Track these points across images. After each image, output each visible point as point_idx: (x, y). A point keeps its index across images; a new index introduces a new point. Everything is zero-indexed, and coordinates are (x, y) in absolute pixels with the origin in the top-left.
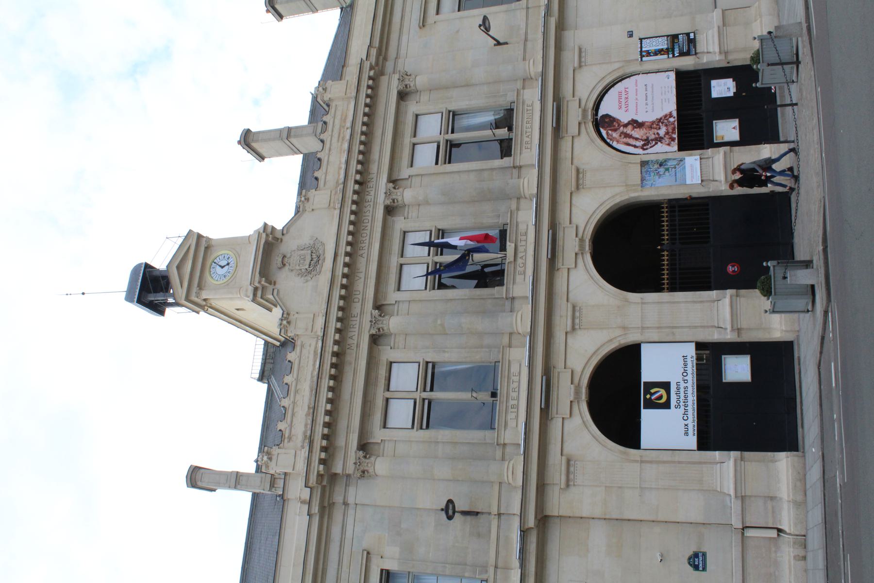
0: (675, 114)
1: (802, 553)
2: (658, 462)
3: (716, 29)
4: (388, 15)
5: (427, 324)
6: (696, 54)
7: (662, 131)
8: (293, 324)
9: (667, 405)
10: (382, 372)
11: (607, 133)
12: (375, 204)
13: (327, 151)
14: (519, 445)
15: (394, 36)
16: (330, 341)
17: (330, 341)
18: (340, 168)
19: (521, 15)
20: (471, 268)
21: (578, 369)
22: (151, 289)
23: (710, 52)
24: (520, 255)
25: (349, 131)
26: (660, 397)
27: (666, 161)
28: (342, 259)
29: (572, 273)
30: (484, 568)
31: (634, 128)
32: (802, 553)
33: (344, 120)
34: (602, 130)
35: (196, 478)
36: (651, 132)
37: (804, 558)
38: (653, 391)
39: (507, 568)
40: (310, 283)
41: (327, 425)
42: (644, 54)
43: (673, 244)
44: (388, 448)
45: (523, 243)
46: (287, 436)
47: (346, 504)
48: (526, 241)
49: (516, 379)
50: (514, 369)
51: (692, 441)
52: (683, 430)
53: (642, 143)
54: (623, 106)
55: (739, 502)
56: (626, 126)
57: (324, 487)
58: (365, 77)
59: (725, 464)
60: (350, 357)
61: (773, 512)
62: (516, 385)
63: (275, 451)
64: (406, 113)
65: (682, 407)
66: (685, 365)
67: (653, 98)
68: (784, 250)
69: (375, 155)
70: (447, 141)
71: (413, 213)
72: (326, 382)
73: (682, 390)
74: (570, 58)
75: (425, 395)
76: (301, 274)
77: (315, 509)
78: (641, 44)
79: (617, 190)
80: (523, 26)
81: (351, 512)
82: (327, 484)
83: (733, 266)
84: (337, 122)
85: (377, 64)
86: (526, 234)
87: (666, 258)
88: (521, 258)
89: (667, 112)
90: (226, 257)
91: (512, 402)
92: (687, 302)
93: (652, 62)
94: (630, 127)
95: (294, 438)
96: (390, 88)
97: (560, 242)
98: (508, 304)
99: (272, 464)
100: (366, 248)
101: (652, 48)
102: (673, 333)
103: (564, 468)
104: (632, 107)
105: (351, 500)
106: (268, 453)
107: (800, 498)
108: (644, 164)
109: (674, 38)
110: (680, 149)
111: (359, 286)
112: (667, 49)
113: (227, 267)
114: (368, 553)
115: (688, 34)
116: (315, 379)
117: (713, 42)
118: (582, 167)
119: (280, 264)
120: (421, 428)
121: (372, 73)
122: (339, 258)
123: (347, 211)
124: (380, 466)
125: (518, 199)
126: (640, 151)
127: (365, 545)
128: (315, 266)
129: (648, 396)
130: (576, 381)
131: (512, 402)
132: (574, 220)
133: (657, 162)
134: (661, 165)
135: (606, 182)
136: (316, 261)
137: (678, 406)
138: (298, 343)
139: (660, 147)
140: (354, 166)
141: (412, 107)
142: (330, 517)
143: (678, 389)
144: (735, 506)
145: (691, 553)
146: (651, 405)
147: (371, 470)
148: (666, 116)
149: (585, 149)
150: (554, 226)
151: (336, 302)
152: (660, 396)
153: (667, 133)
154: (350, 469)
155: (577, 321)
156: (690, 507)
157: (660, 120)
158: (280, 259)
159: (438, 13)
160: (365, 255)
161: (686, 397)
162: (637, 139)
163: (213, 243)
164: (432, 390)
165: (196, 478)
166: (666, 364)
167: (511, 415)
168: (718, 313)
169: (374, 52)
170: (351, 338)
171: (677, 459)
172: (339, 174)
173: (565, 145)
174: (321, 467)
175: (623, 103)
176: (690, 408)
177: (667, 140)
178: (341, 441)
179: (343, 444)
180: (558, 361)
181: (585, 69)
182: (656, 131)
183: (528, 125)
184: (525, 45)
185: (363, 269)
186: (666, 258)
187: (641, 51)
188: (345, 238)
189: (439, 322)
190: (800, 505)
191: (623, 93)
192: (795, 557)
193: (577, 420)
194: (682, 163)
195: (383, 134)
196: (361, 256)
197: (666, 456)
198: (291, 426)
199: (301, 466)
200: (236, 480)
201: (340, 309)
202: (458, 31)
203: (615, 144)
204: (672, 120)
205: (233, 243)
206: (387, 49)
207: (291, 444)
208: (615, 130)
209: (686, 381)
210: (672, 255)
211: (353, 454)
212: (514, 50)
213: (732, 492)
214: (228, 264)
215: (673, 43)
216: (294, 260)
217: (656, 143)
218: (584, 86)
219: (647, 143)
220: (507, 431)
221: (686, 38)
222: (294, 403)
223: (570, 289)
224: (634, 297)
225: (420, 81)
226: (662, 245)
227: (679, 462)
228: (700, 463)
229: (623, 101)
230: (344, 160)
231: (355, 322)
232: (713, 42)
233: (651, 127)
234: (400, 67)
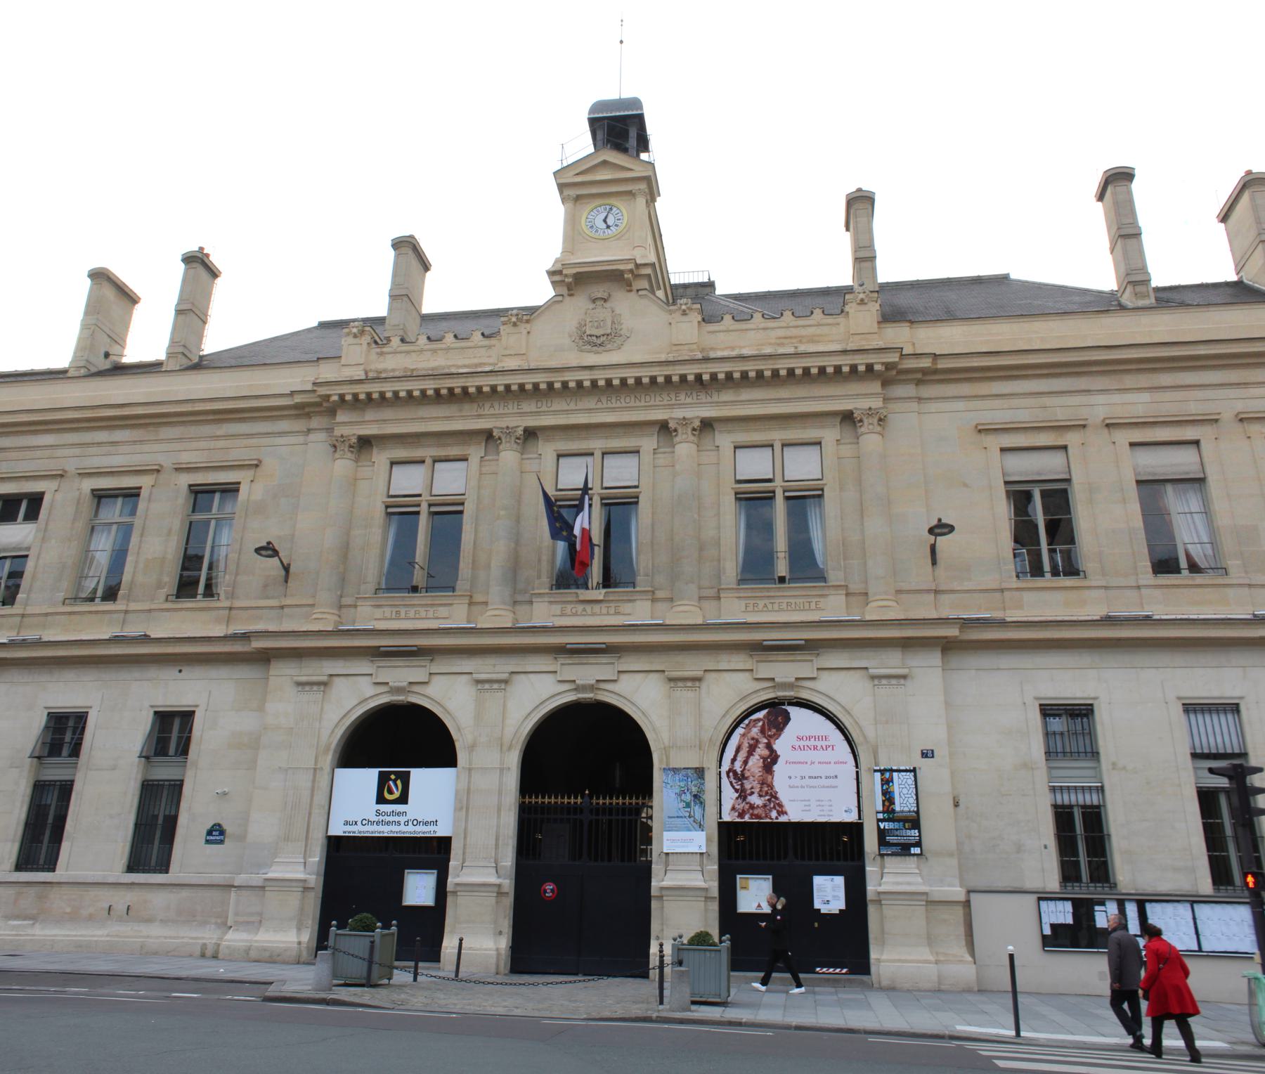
0: (783, 819)
1: (209, 952)
4: (1001, 374)
5: (498, 494)
6: (882, 855)
7: (755, 800)
9: (381, 800)
10: (454, 451)
11: (759, 720)
12: (671, 406)
13: (763, 325)
16: (493, 381)
17: (493, 381)
18: (733, 348)
19: (990, 581)
20: (590, 547)
21: (429, 690)
22: (620, 129)
23: (886, 877)
24: (588, 608)
25: (792, 350)
26: (391, 792)
27: (702, 804)
28: (586, 377)
29: (550, 677)
31: (764, 759)
32: (209, 952)
33: (812, 340)
34: (765, 712)
35: (860, 205)
36: (755, 784)
37: (203, 956)
38: (399, 782)
42: (887, 775)
43: (591, 811)
45: (604, 611)
46: (385, 350)
47: (309, 431)
48: (608, 614)
49: (430, 614)
50: (443, 611)
51: (337, 830)
52: (350, 819)
53: (739, 770)
54: (802, 743)
55: (260, 884)
56: (769, 746)
57: (318, 404)
59: (303, 867)
61: (248, 923)
62: (423, 614)
63: (366, 339)
64: (822, 427)
65: (376, 819)
66: (426, 823)
67: (814, 783)
68: (434, 955)
69: (746, 394)
70: (774, 492)
71: (846, 450)
72: (430, 386)
73: (396, 818)
74: (891, 661)
75: (424, 509)
76: (581, 326)
78: (906, 771)
79: (665, 736)
80: (967, 585)
81: (301, 439)
82: (317, 408)
83: (552, 891)
84: (811, 331)
85: (900, 372)
86: (617, 613)
87: (572, 801)
88: (584, 610)
89: (788, 807)
90: (618, 222)
91: (403, 611)
92: (498, 826)
93: (874, 785)
94: (766, 752)
95: (381, 359)
96: (861, 397)
97: (592, 659)
99: (351, 340)
100: (610, 405)
101: (896, 788)
102: (467, 806)
103: (314, 679)
104: (800, 756)
105: (312, 437)
106: (362, 332)
107: (253, 954)
108: (700, 772)
109: (914, 822)
110: (724, 828)
111: (559, 404)
112: (893, 811)
113: (604, 226)
115: (918, 844)
116: (447, 371)
117: (898, 883)
118: (704, 685)
120: (387, 507)
122: (587, 372)
124: (343, 465)
126: (726, 766)
128: (589, 343)
129: (393, 777)
130: (416, 688)
131: (403, 611)
132: (825, 675)
133: (701, 791)
134: (695, 796)
135: (678, 718)
136: (595, 342)
137: (378, 813)
139: (729, 795)
140: (737, 368)
141: (830, 434)
142: (297, 417)
143: (399, 814)
144: (256, 879)
145: (225, 827)
146: (383, 780)
147: (337, 455)
148: (780, 805)
149: (731, 688)
150: (811, 647)
151: (529, 380)
152: (392, 792)
153: (752, 807)
154: (338, 431)
155: (487, 686)
157: (774, 796)
158: (599, 296)
159: (1132, 445)
161: (388, 823)
162: (745, 762)
164: (788, 498)
165: (860, 205)
166: (431, 799)
167: (387, 611)
168: (485, 865)
169: (926, 363)
171: (316, 811)
172: (723, 349)
173: (739, 660)
174: (335, 398)
175: (808, 743)
176: (375, 828)
177: (741, 806)
178: (370, 415)
180: (440, 665)
181: (868, 684)
182: (757, 790)
183: (784, 606)
184: (928, 591)
185: (581, 405)
186: (572, 801)
187: (892, 771)
189: (502, 513)
190: (248, 956)
191: (824, 743)
192: (205, 945)
193: (369, 691)
194: (697, 826)
195: (779, 400)
197: (320, 798)
199: (348, 373)
200: (864, 258)
201: (508, 387)
202: (965, 485)
203: (740, 731)
204: (774, 814)
208: (762, 731)
210: (575, 809)
211: (351, 432)
214: (608, 227)
215: (904, 820)
216: (602, 313)
217: (737, 791)
218: (840, 685)
219: (738, 777)
220: (369, 608)
221: (913, 840)
223: (531, 676)
224: (514, 760)
225: (871, 441)
226: (591, 796)
228: (307, 838)
229: (812, 743)
230: (746, 352)
231: (512, 408)
232: (898, 883)
233: (763, 783)
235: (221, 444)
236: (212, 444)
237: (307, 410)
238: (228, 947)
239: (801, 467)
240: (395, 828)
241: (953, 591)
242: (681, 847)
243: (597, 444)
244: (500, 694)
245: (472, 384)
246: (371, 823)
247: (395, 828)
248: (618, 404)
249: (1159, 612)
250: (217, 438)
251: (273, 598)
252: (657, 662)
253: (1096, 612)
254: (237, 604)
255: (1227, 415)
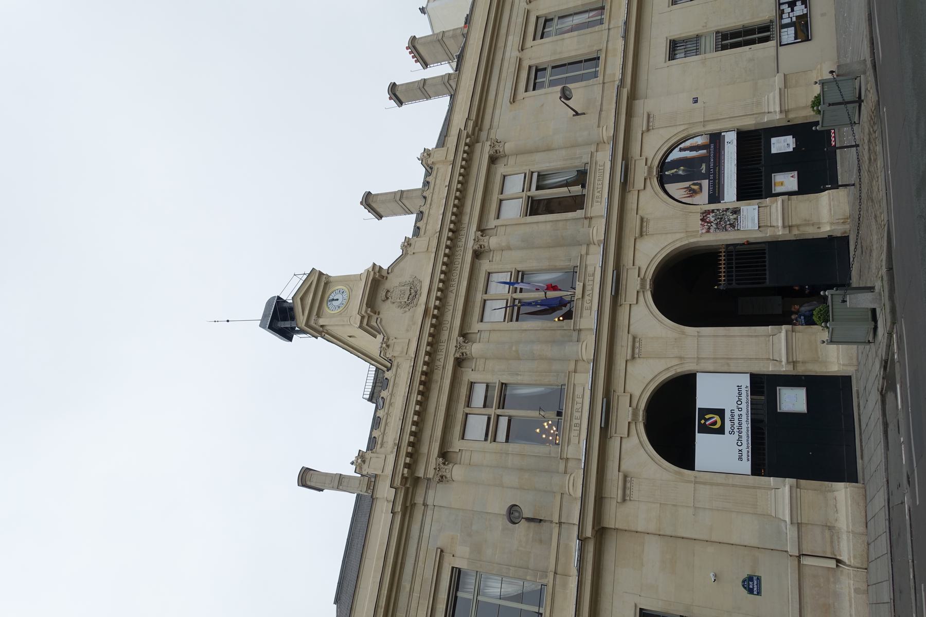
2: (712, 484)
3: (777, 91)
8: (391, 348)
9: (721, 431)
10: (464, 391)
12: (465, 249)
14: (580, 460)
15: (489, 111)
17: (422, 353)
19: (598, 89)
21: (637, 394)
22: (282, 319)
24: (587, 293)
26: (715, 423)
29: (634, 308)
30: (545, 573)
35: (307, 479)
38: (707, 417)
39: (567, 575)
40: (408, 314)
41: (409, 455)
44: (465, 456)
45: (591, 283)
47: (425, 505)
49: (580, 400)
50: (579, 391)
55: (795, 528)
57: (407, 490)
58: (436, 280)
59: (780, 491)
60: (437, 376)
62: (579, 406)
64: (479, 270)
65: (737, 434)
66: (740, 394)
69: (467, 209)
71: (497, 257)
72: (415, 397)
73: (736, 417)
74: (639, 123)
76: (400, 307)
77: (398, 508)
81: (429, 512)
86: (593, 275)
87: (723, 270)
91: (575, 421)
98: (575, 334)
102: (725, 366)
114: (442, 551)
119: (383, 297)
121: (468, 140)
123: (441, 253)
124: (457, 472)
125: (588, 245)
127: (439, 544)
128: (413, 299)
129: (703, 422)
136: (413, 295)
138: (395, 364)
142: (411, 516)
143: (732, 416)
144: (791, 533)
146: (705, 429)
147: (449, 476)
150: (626, 157)
154: (431, 474)
155: (637, 351)
156: (745, 530)
160: (454, 291)
161: (740, 424)
163: (331, 279)
165: (307, 479)
167: (574, 433)
169: (471, 124)
170: (439, 360)
176: (744, 435)
178: (424, 449)
179: (426, 451)
181: (652, 132)
185: (452, 303)
188: (438, 276)
192: (855, 590)
193: (634, 439)
196: (451, 291)
198: (384, 434)
200: (339, 482)
201: (414, 423)
205: (346, 280)
206: (482, 121)
207: (383, 450)
209: (740, 409)
212: (591, 119)
213: (788, 519)
216: (395, 295)
222: (388, 414)
225: (508, 147)
227: (733, 486)
228: (754, 488)
231: (443, 347)
234: (492, 136)
235: (417, 587)
236: (416, 595)
237: (408, 504)
238: (855, 557)
239: (515, 185)
240: (744, 419)
241: (602, 104)
242: (755, 221)
243: (479, 297)
244: (643, 342)
245: (421, 367)
246: (740, 437)
247: (744, 419)
248: (442, 360)
249: (623, 17)
250: (411, 590)
251: (551, 535)
252: (628, 243)
253: (620, 43)
254: (552, 567)
255: (519, 55)
